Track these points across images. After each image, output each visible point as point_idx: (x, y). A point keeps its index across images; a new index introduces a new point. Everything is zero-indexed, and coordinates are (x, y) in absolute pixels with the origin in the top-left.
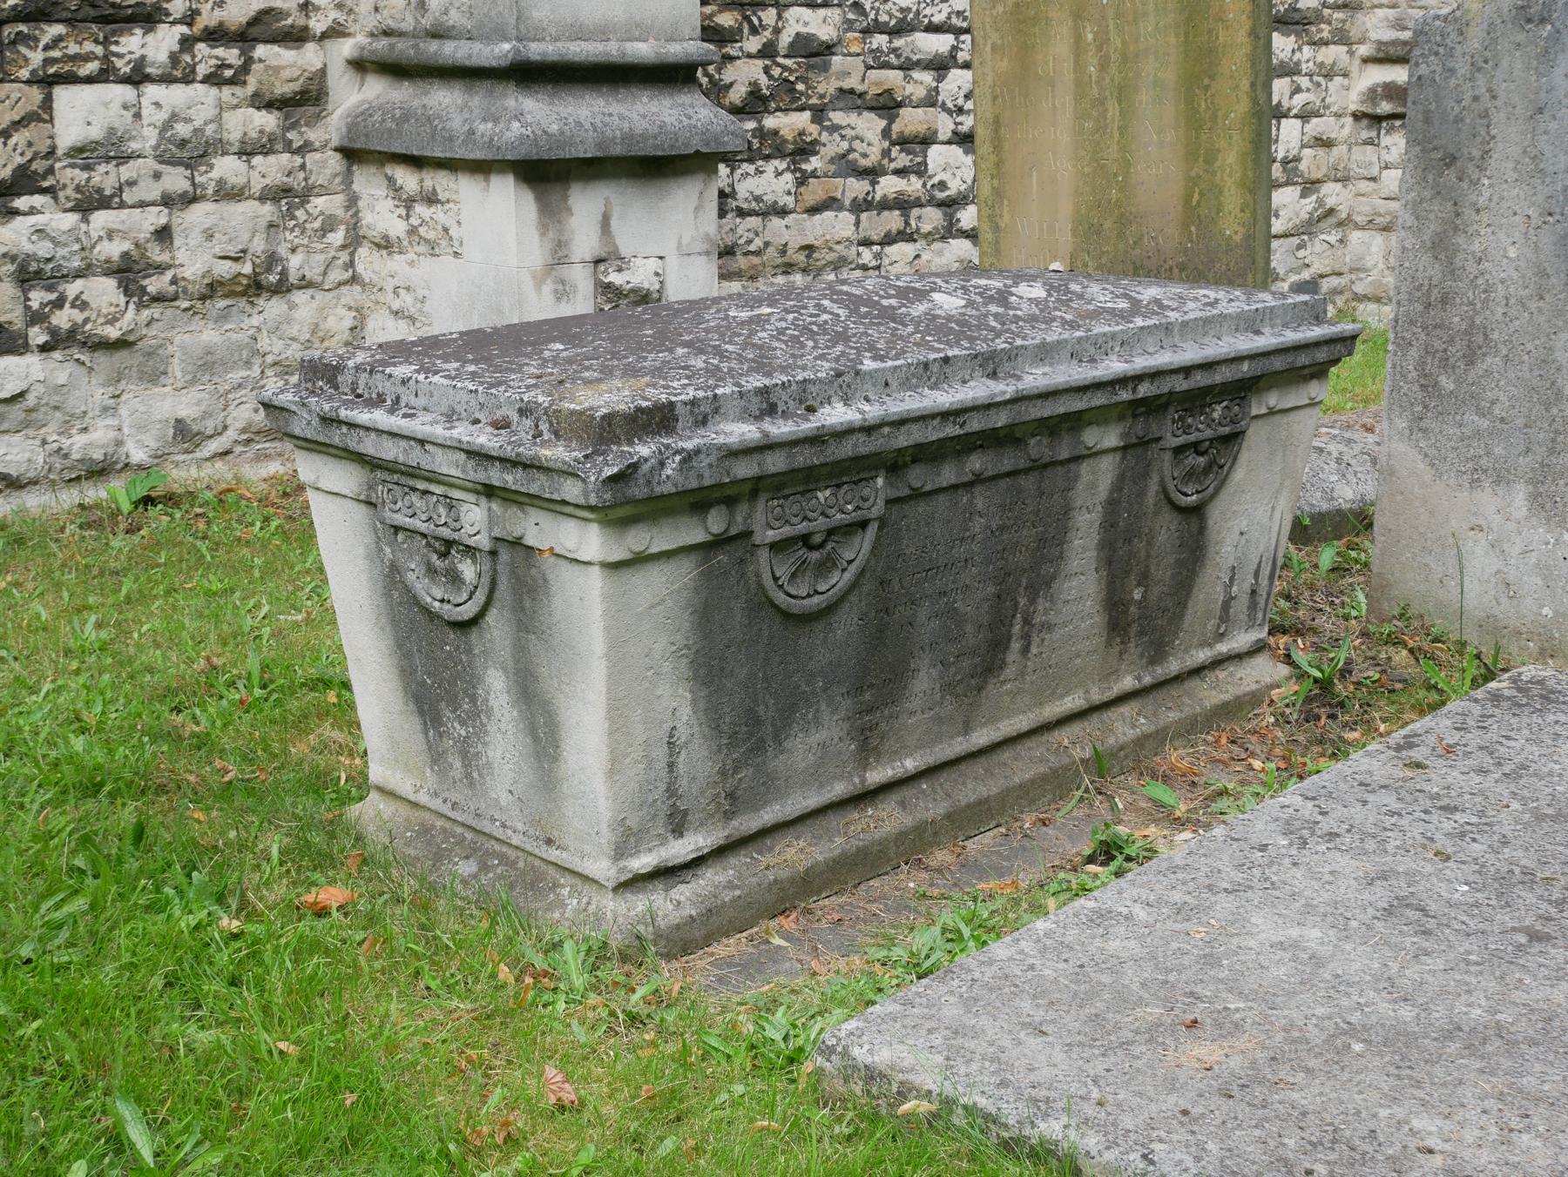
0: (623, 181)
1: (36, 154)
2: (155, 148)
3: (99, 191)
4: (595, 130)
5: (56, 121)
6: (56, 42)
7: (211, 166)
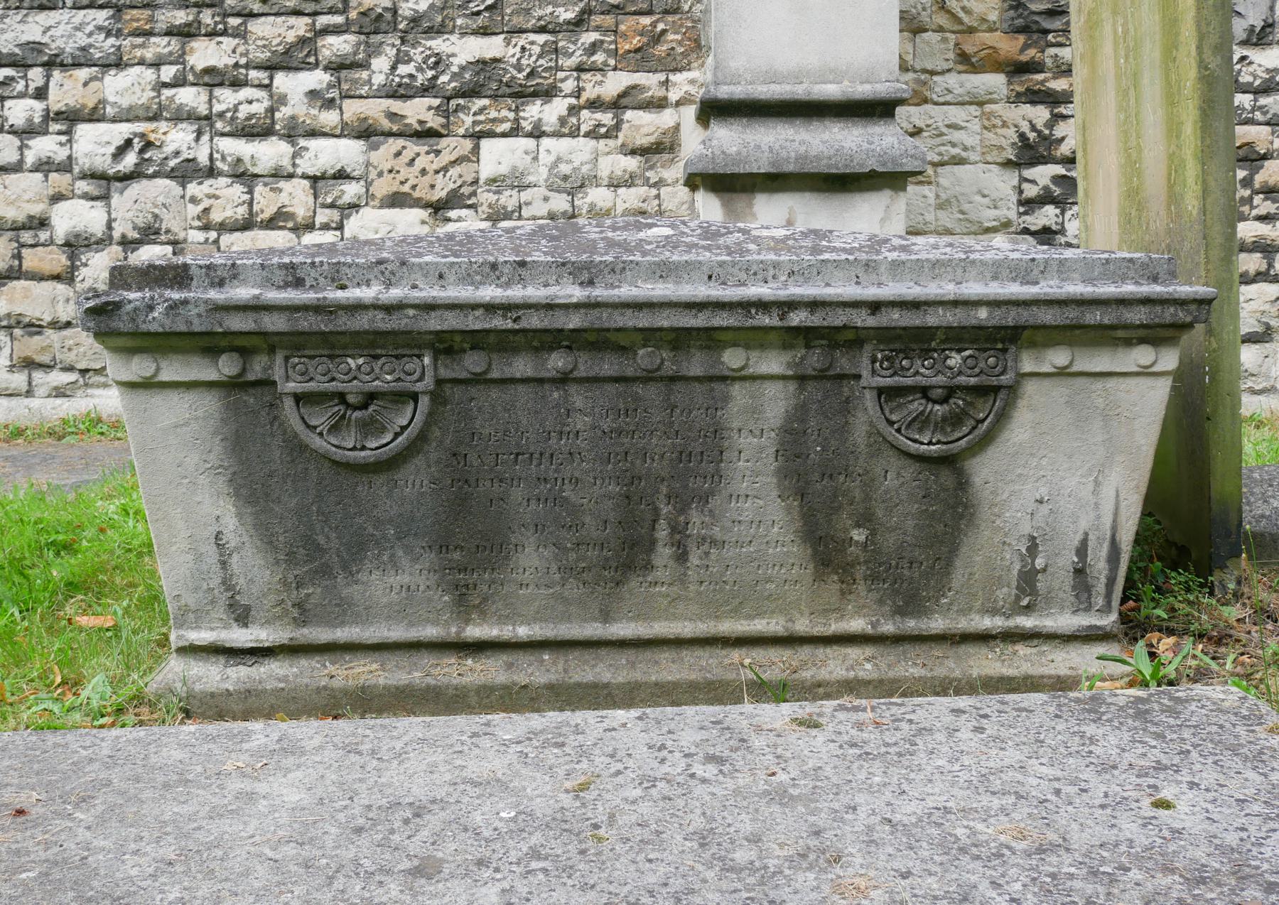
0: (807, 195)
1: (464, 182)
2: (546, 181)
3: (504, 207)
4: (771, 151)
5: (482, 162)
6: (482, 110)
7: (587, 194)
